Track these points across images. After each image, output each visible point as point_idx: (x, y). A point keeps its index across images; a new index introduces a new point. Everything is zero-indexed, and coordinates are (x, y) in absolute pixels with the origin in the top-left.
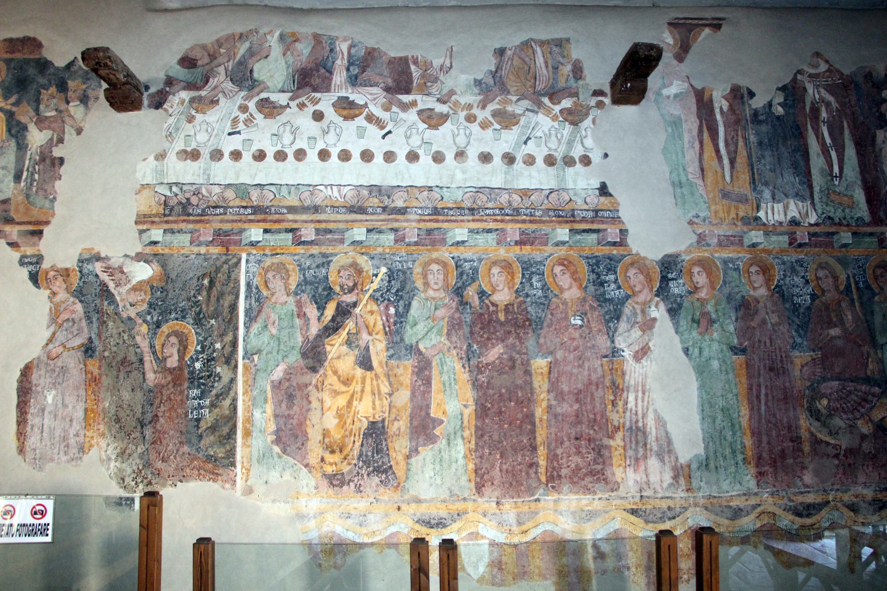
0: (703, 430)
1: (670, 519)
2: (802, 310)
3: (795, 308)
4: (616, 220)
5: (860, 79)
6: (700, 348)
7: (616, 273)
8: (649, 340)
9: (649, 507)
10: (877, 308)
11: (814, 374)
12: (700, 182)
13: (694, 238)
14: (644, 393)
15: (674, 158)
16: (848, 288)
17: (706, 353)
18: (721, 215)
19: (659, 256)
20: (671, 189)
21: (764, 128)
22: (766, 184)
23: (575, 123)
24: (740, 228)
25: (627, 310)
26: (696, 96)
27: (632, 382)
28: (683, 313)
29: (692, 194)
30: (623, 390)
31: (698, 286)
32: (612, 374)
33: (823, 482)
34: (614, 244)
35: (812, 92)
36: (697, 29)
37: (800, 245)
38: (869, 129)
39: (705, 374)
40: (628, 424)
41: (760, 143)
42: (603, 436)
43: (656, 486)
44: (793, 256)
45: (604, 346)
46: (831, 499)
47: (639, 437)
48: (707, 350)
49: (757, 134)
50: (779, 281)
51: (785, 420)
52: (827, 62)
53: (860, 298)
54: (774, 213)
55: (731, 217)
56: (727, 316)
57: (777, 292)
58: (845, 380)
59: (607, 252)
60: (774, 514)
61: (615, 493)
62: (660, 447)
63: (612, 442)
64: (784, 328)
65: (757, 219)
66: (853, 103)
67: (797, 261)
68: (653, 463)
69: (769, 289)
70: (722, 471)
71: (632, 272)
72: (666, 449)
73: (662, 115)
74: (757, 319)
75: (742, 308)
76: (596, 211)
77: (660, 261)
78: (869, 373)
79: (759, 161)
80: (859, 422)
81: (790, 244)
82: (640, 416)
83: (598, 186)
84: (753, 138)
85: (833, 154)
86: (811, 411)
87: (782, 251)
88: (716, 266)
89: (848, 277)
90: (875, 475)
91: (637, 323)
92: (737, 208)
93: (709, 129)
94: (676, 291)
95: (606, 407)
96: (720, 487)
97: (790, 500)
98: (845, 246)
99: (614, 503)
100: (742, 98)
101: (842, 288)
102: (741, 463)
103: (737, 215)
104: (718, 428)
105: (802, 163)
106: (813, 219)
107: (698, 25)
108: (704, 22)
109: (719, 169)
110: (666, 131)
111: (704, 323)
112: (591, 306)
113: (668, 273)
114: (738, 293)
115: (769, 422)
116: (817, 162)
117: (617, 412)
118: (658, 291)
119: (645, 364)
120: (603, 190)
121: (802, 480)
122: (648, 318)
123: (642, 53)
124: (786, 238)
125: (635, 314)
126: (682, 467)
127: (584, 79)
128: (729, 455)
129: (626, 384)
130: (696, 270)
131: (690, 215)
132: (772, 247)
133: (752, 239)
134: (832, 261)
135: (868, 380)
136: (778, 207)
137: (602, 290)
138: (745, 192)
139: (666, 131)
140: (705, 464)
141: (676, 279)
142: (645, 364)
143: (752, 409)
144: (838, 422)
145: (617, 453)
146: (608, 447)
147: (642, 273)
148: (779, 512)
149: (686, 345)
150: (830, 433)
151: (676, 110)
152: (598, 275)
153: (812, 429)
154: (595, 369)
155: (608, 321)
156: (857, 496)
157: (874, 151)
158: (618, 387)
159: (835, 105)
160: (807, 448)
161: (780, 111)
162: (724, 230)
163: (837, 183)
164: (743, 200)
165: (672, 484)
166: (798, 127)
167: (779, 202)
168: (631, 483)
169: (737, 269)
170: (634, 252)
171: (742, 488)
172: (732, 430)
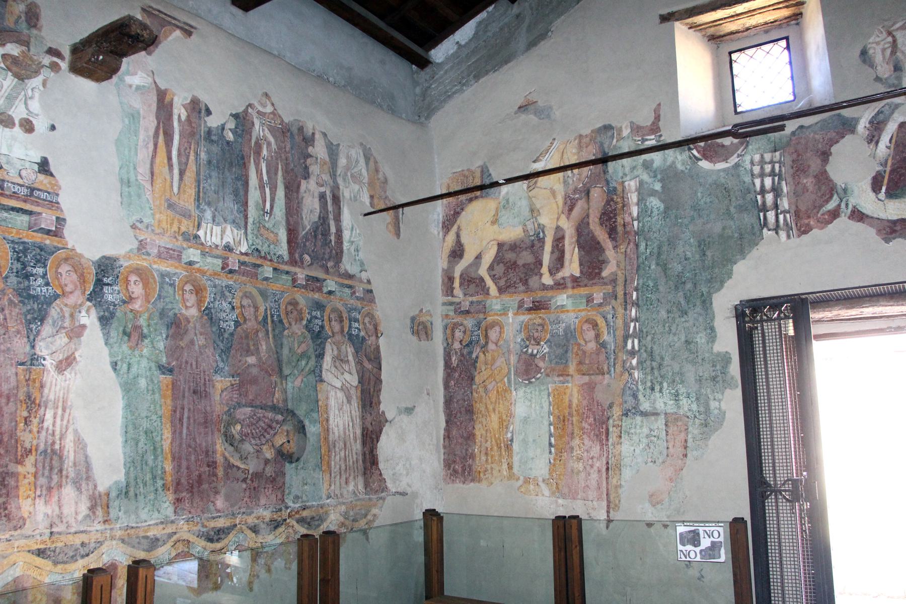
0: (125, 453)
1: (83, 557)
2: (226, 335)
3: (221, 332)
4: (54, 205)
5: (294, 129)
6: (129, 364)
7: (45, 266)
8: (76, 350)
9: (60, 545)
10: (285, 341)
11: (231, 399)
12: (148, 186)
13: (135, 244)
14: (64, 410)
15: (126, 152)
16: (265, 319)
17: (134, 370)
18: (164, 225)
19: (96, 257)
20: (119, 185)
21: (215, 149)
22: (209, 204)
23: (21, 78)
24: (180, 243)
25: (54, 312)
26: (158, 95)
27: (52, 397)
28: (115, 323)
29: (139, 196)
30: (39, 405)
31: (133, 296)
32: (28, 385)
33: (232, 506)
34: (48, 232)
35: (259, 129)
36: (168, 27)
37: (231, 272)
38: (296, 176)
39: (132, 392)
40: (42, 447)
41: (209, 162)
42: (10, 461)
43: (69, 519)
44: (225, 281)
45: (22, 351)
46: (237, 522)
47: (54, 462)
48: (136, 367)
49: (208, 152)
50: (209, 303)
51: (204, 444)
52: (273, 105)
53: (274, 330)
54: (215, 234)
55: (173, 230)
56: (158, 333)
57: (207, 315)
58: (256, 407)
59: (38, 240)
60: (189, 541)
61: (19, 531)
62: (78, 474)
63: (20, 469)
64: (209, 351)
65: (196, 237)
66: (287, 149)
67: (227, 286)
68: (68, 491)
69: (199, 310)
70: (141, 498)
71: (64, 269)
72: (85, 475)
73: (121, 103)
74: (187, 339)
75: (174, 326)
76: (32, 190)
77: (97, 261)
78: (275, 401)
79: (206, 180)
80: (264, 447)
81: (223, 268)
82: (57, 437)
83: (39, 161)
84: (203, 155)
85: (267, 190)
86: (226, 436)
87: (215, 274)
88: (154, 278)
89: (266, 309)
90: (273, 497)
91: (64, 328)
92: (180, 222)
93: (165, 133)
94: (110, 298)
95: (16, 425)
96: (138, 516)
97: (204, 526)
98: (266, 279)
99: (16, 544)
100: (200, 112)
101: (260, 318)
102: (160, 489)
103: (179, 228)
104: (140, 452)
105: (242, 193)
106: (244, 248)
107: (170, 23)
108: (176, 22)
109: (168, 177)
110: (123, 122)
111: (135, 337)
112: (10, 299)
113: (104, 276)
114: (171, 310)
115: (190, 446)
116: (254, 195)
117: (30, 432)
118: (90, 294)
119: (68, 376)
120: (44, 166)
121: (215, 505)
122: (77, 324)
123: (135, 29)
124: (219, 262)
125: (63, 317)
126: (100, 496)
127: (40, 30)
128: (149, 482)
129: (44, 399)
130: (133, 278)
131: (134, 218)
132: (206, 268)
133: (189, 257)
134: (255, 292)
135: (274, 408)
136: (217, 230)
137: (26, 283)
138: (190, 208)
139: (123, 122)
140: (125, 492)
141: (111, 285)
142: (68, 376)
143: (174, 433)
144: (248, 447)
145: (27, 481)
146: (15, 475)
147: (76, 271)
148: (193, 538)
149: (115, 359)
150: (241, 458)
151: (136, 102)
152: (24, 266)
153: (227, 454)
154: (8, 378)
155: (30, 322)
156: (258, 518)
157: (297, 198)
158: (34, 402)
159: (274, 146)
160: (220, 472)
161: (230, 136)
162: (166, 242)
163: (267, 219)
164: (186, 215)
165: (88, 516)
166: (243, 158)
167: (218, 224)
168: (40, 517)
169: (172, 285)
170: (70, 246)
171: (160, 516)
172: (154, 455)
